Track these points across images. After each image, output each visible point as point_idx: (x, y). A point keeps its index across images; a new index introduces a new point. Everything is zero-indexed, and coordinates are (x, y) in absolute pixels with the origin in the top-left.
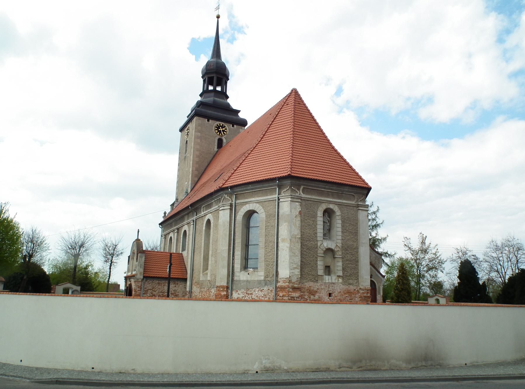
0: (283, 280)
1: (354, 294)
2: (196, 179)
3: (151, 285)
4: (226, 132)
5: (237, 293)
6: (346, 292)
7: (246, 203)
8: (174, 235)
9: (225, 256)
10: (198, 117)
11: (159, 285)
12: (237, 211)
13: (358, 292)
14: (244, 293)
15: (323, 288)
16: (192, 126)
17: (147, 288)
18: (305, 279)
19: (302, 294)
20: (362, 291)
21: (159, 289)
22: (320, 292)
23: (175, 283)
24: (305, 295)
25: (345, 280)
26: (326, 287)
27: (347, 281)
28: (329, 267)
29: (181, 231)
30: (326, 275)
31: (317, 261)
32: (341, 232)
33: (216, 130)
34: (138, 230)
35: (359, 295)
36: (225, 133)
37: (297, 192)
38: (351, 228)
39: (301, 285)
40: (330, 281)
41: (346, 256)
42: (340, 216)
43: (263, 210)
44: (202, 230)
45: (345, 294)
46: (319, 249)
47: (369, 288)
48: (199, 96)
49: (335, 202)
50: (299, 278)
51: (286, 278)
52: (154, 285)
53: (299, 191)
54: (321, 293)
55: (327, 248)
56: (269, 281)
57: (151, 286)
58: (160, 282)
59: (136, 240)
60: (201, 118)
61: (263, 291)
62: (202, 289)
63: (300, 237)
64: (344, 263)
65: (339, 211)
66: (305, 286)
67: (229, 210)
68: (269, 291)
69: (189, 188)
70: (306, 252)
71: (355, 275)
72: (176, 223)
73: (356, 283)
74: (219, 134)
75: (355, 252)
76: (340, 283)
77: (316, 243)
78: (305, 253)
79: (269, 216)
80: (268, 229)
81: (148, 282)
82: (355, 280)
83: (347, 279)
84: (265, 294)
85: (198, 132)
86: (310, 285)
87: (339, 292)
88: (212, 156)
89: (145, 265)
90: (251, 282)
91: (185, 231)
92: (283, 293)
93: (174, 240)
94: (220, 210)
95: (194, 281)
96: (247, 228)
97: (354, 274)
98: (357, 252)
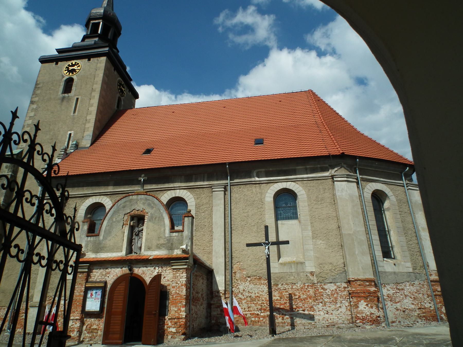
9: (363, 239)
67: (223, 192)
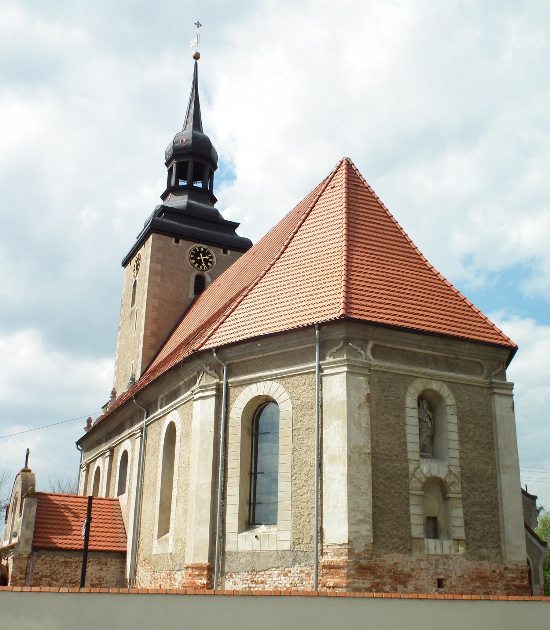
0: (334, 550)
1: (492, 581)
2: (153, 353)
3: (48, 565)
4: (211, 262)
5: (231, 580)
6: (475, 577)
7: (251, 382)
8: (104, 462)
10: (156, 235)
11: (66, 567)
12: (231, 399)
13: (502, 576)
14: (247, 580)
15: (423, 567)
16: (146, 252)
17: (40, 574)
18: (384, 545)
19: (378, 581)
20: (510, 575)
21: (65, 575)
22: (417, 577)
23: (100, 563)
24: (384, 584)
25: (471, 550)
26: (431, 564)
27: (477, 551)
28: (434, 519)
29: (118, 453)
30: (428, 537)
31: (408, 505)
32: (457, 442)
33: (192, 259)
34: (28, 450)
35: (504, 582)
36: (209, 264)
37: (361, 354)
38: (478, 434)
39: (376, 561)
40: (439, 551)
41: (472, 496)
42: (454, 407)
43: (286, 396)
44: (159, 446)
45: (472, 580)
46: (411, 478)
47: (525, 568)
48: (160, 198)
49: (441, 376)
50: (371, 545)
51: (341, 545)
52: (55, 566)
53: (365, 352)
54: (421, 578)
55: (429, 476)
56: (302, 551)
57: (49, 568)
58: (68, 560)
59: (23, 471)
60: (162, 236)
61: (289, 575)
62: (156, 575)
63: (369, 451)
64: (467, 511)
65: (452, 396)
66: (383, 563)
68: (303, 574)
69: (137, 371)
70: (384, 485)
71: (492, 537)
72: (109, 437)
73: (497, 556)
74: (199, 267)
75: (491, 485)
76: (461, 556)
77: (405, 464)
78: (382, 487)
79: (299, 408)
80: (299, 435)
81: (42, 561)
82: (493, 548)
83: (475, 547)
84: (294, 582)
85: (157, 263)
86: (396, 561)
87: (461, 577)
88: (183, 308)
89: (36, 522)
90: (262, 555)
91: (125, 453)
92: (335, 580)
93: (103, 474)
94: (194, 398)
95: (141, 558)
96: (252, 435)
97: (490, 535)
98: (495, 486)
